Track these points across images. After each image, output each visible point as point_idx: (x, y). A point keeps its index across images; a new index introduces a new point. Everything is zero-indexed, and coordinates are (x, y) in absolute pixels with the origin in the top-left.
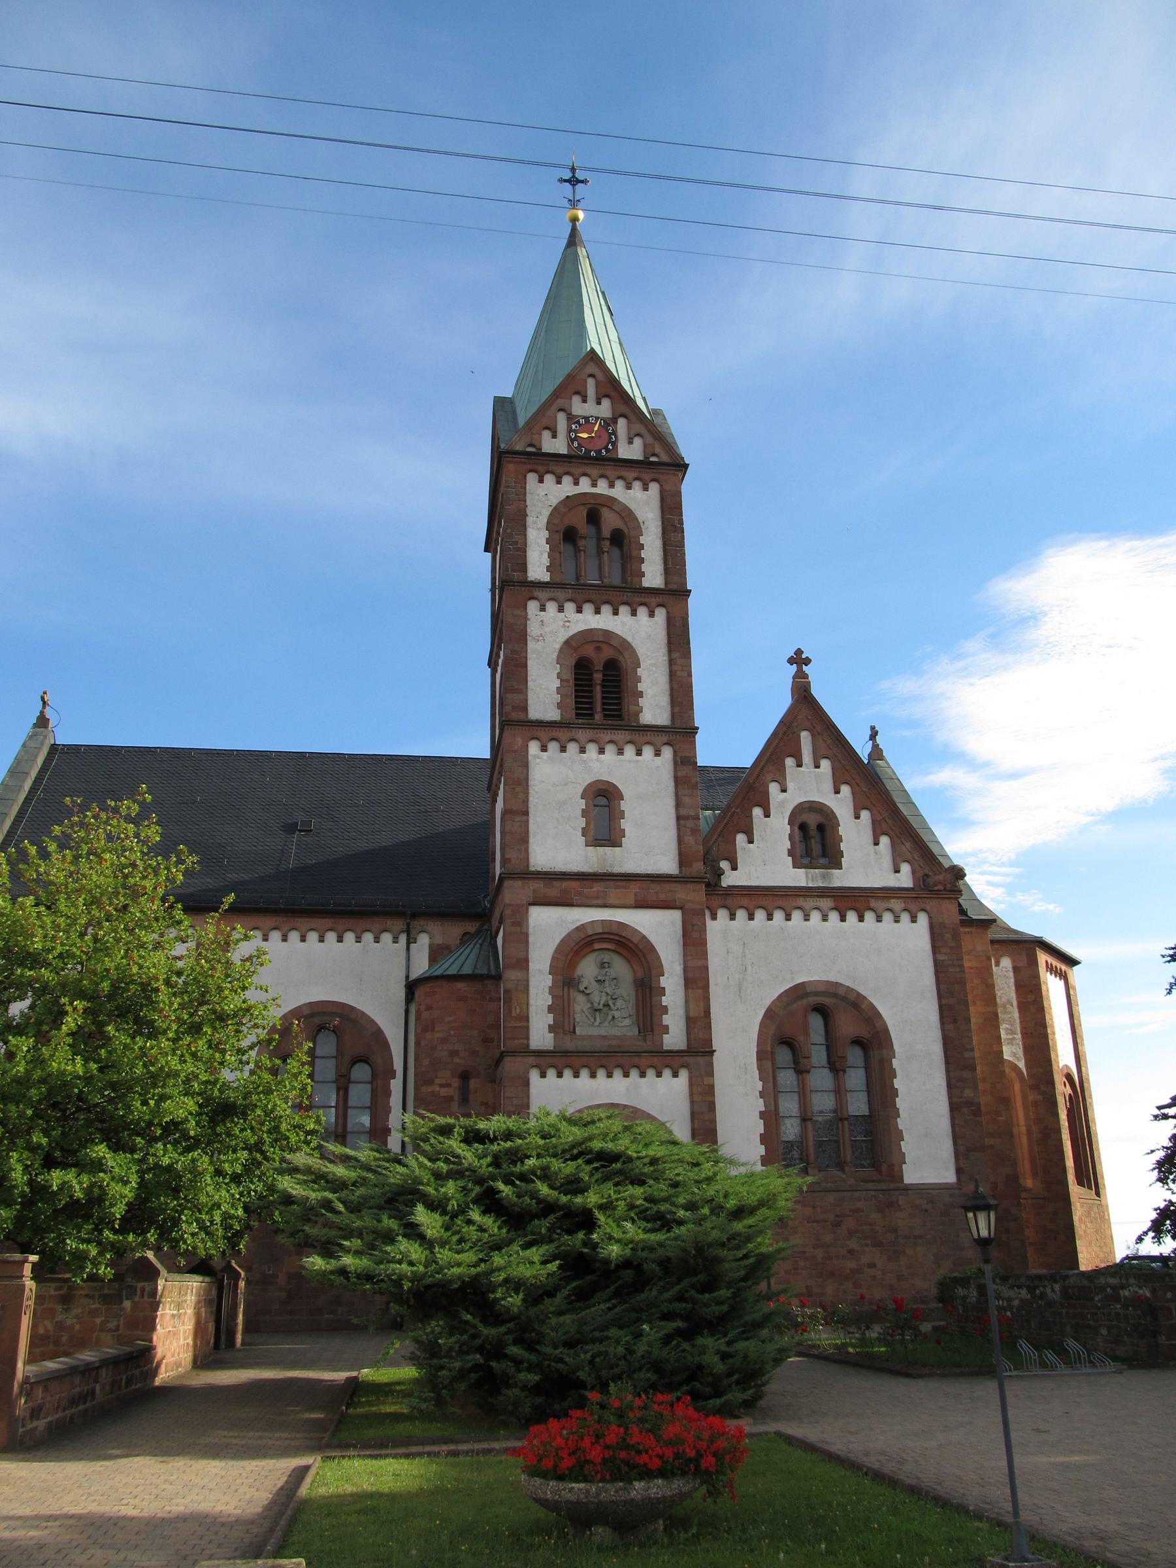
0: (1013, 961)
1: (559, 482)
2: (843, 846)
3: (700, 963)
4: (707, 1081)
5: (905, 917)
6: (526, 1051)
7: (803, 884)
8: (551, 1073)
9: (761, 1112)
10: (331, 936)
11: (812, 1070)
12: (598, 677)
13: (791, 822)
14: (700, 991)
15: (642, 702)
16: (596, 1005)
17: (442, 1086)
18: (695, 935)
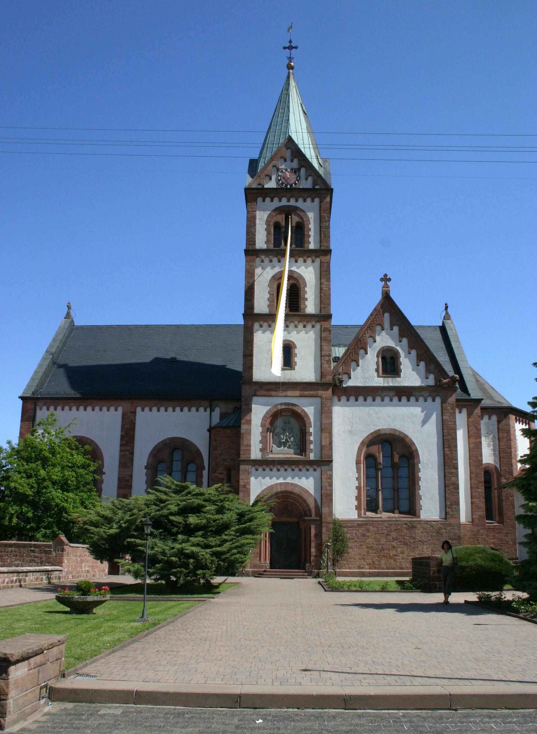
0: (498, 417)
1: (272, 201)
2: (402, 367)
7: (382, 385)
9: (356, 487)
10: (178, 409)
11: (400, 468)
14: (328, 434)
15: (306, 303)
17: (219, 474)
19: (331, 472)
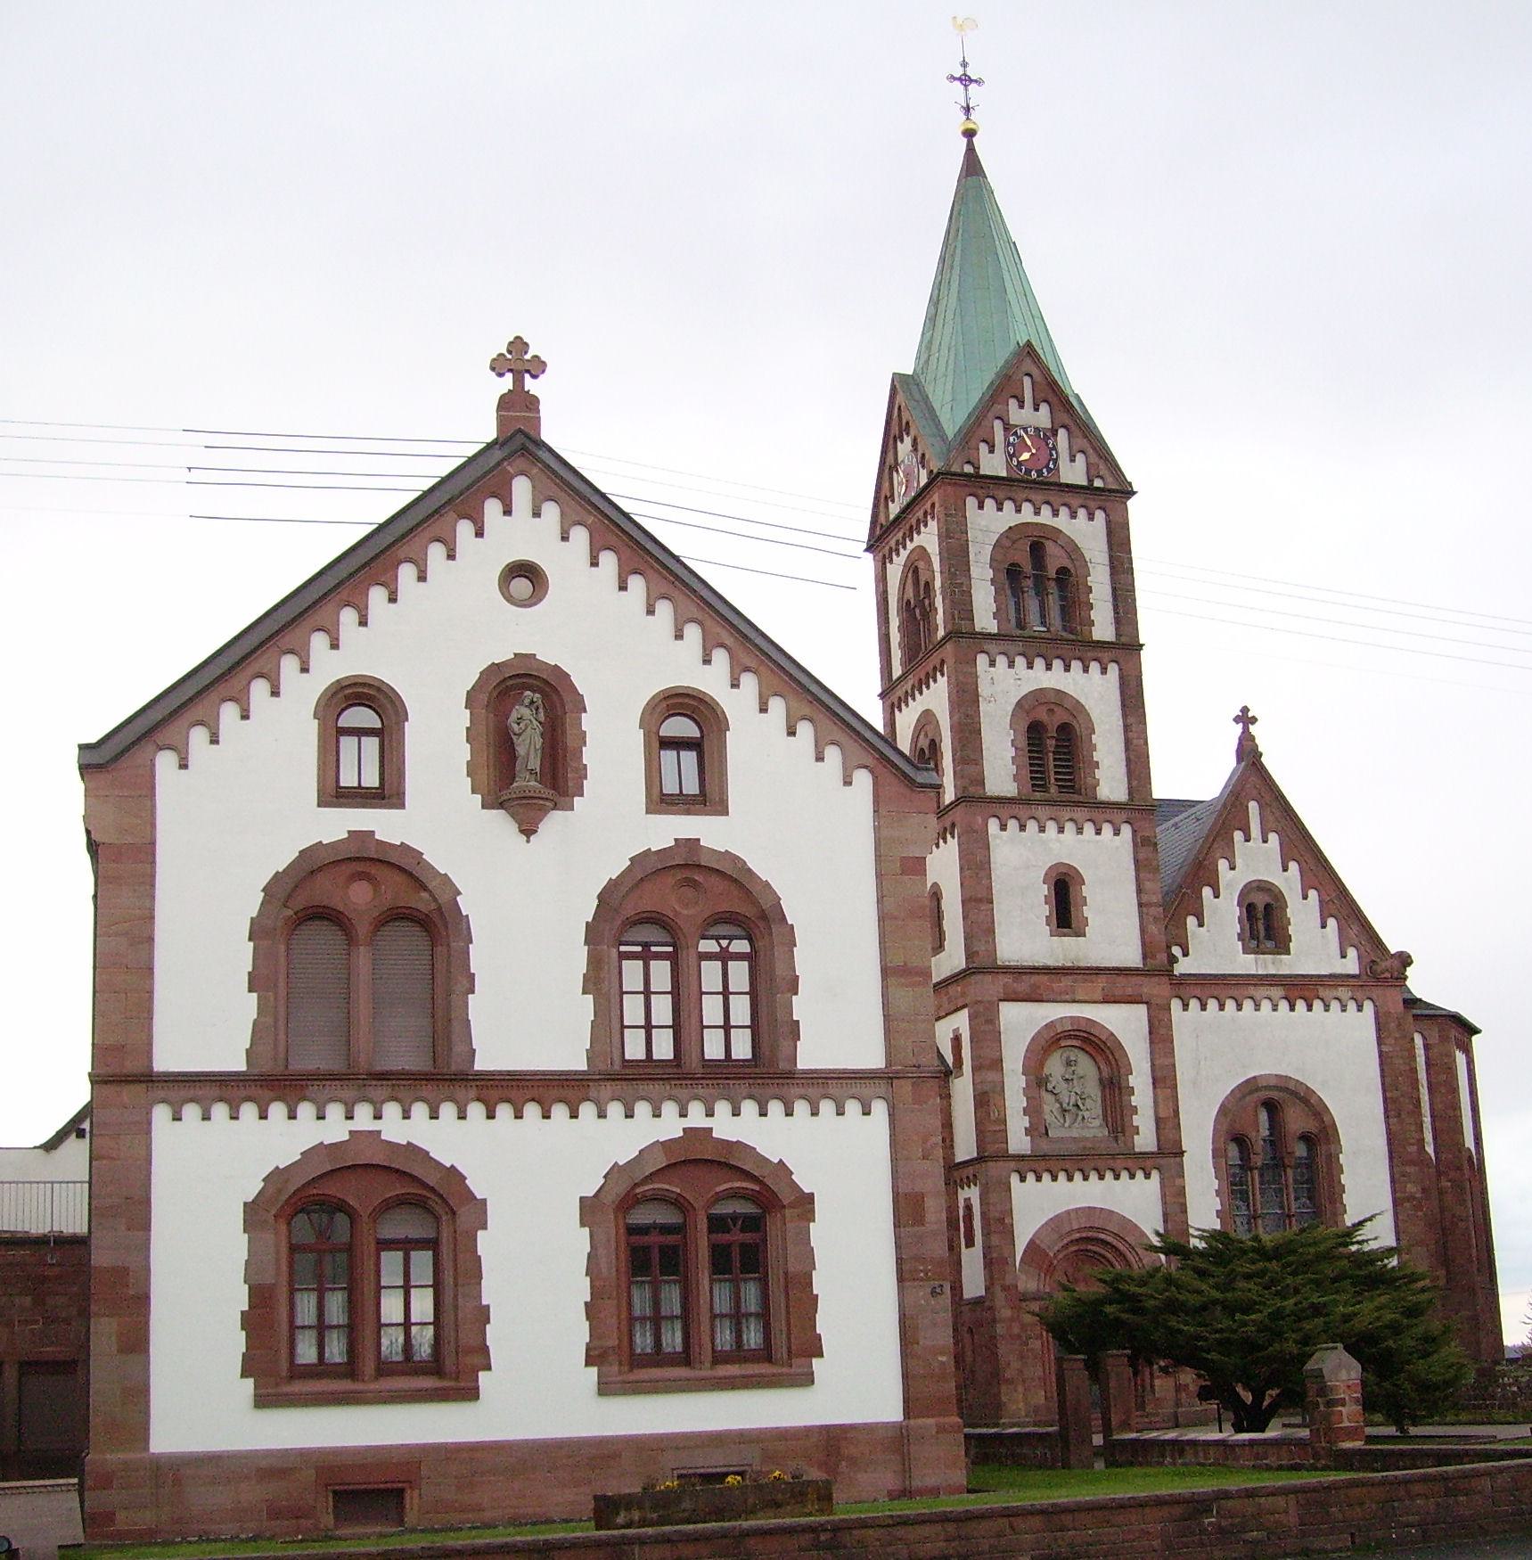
2: (1291, 930)
3: (1171, 1060)
4: (1178, 1181)
5: (1352, 1006)
6: (1005, 1156)
8: (1031, 1177)
12: (1051, 743)
13: (1239, 904)
15: (1098, 773)
16: (1065, 1105)
18: (1163, 1031)
19: (1182, 1179)
